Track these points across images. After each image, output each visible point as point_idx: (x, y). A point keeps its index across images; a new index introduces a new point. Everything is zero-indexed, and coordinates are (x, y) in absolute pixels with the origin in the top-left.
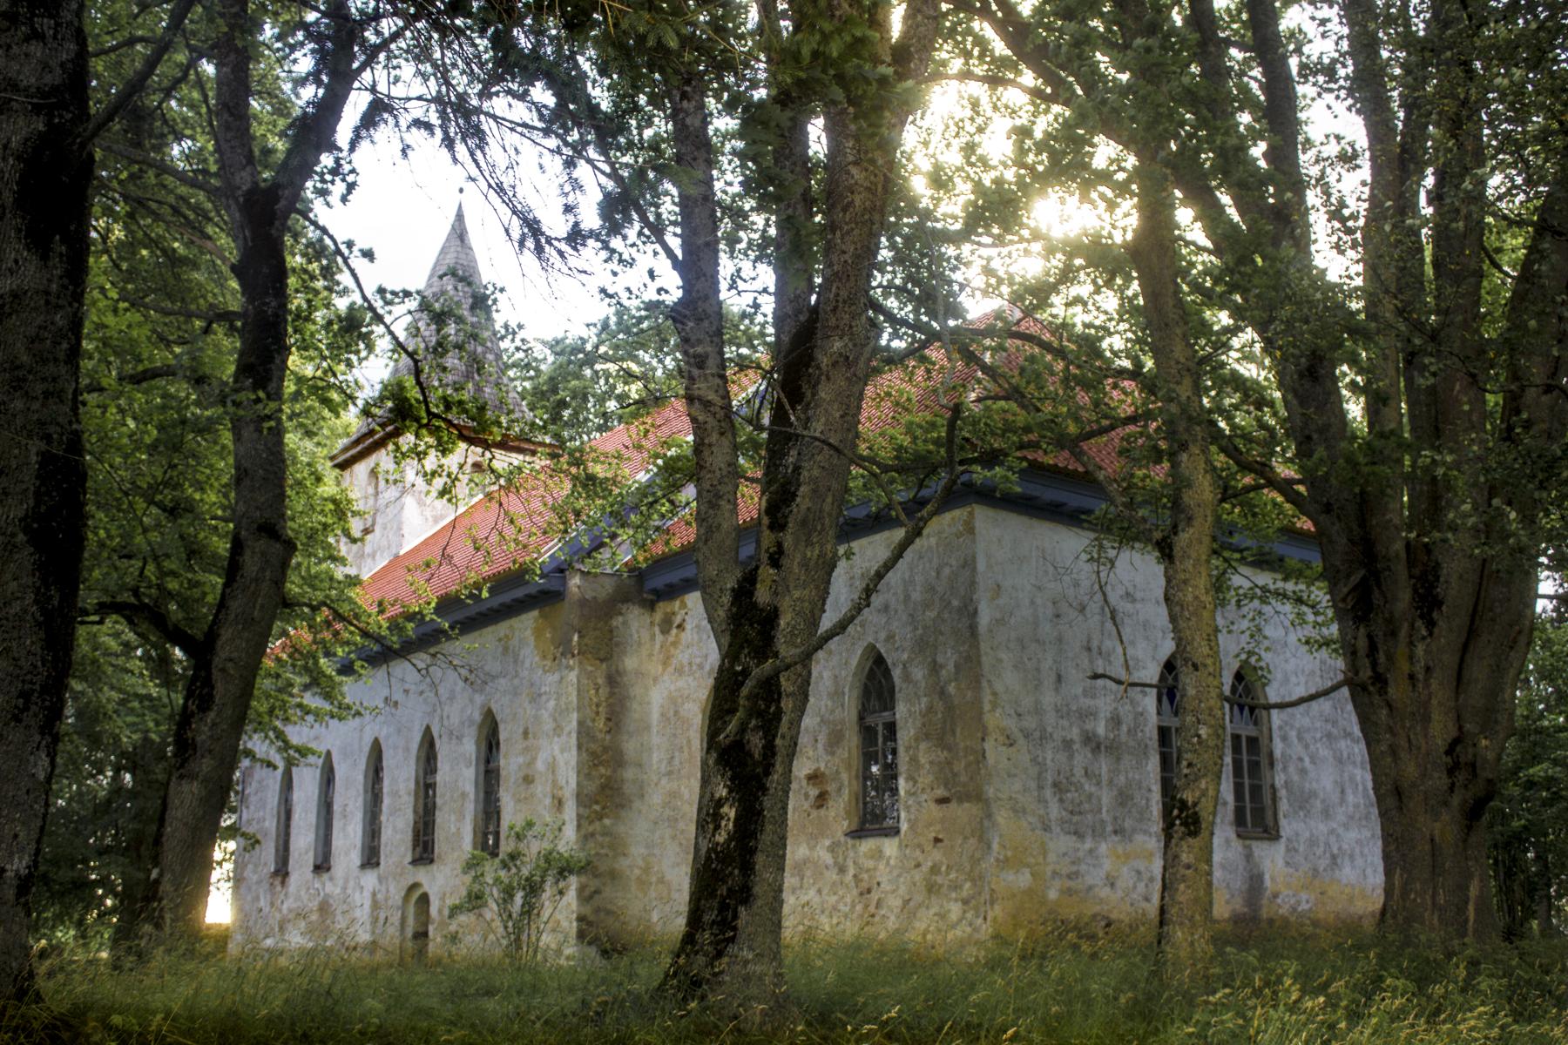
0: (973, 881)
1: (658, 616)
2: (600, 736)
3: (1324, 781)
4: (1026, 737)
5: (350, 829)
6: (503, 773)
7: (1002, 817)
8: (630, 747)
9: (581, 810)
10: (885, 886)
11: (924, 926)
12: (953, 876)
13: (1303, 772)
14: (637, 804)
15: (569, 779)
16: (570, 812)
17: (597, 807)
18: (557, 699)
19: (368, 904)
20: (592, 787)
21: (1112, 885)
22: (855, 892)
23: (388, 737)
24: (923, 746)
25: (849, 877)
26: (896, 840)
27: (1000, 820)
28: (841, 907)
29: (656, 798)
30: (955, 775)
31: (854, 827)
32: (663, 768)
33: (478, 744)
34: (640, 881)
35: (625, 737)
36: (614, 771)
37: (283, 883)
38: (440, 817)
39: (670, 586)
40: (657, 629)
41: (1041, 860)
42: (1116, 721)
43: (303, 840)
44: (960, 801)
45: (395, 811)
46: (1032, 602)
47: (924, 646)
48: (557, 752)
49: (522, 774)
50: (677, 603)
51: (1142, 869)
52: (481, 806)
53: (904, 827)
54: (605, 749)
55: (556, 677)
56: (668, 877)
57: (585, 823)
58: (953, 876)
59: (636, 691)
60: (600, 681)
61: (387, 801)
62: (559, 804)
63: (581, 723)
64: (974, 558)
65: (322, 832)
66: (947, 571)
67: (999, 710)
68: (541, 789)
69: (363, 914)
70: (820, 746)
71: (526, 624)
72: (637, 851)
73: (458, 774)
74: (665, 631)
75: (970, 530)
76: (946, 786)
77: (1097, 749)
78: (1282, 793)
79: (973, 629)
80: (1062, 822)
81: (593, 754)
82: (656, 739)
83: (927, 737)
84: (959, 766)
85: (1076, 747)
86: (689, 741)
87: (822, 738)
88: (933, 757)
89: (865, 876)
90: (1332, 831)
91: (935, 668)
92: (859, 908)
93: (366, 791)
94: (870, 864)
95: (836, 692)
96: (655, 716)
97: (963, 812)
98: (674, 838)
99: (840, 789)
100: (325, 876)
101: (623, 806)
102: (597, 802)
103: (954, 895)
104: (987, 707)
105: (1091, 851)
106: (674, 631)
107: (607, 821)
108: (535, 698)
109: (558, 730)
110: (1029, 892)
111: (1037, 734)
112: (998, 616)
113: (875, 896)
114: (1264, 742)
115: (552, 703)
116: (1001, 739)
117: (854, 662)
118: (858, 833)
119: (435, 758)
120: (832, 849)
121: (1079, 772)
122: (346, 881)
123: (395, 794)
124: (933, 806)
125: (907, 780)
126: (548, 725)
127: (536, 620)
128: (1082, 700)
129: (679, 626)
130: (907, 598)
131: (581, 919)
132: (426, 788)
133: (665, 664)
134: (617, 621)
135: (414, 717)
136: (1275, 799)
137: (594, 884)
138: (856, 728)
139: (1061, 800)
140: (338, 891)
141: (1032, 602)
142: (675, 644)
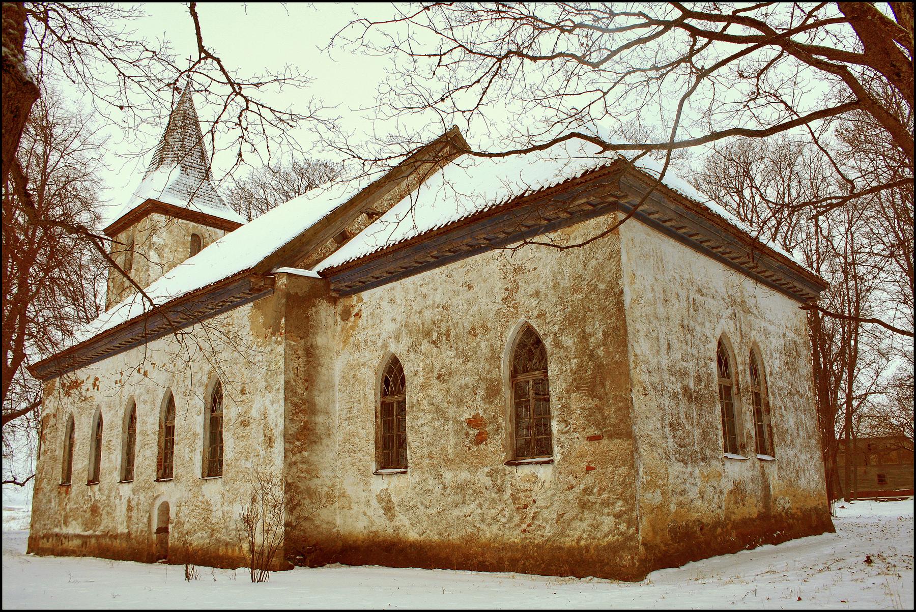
0: (626, 501)
1: (339, 308)
2: (300, 391)
3: (790, 421)
4: (654, 389)
5: (113, 457)
7: (644, 448)
8: (320, 400)
11: (578, 533)
12: (605, 495)
13: (782, 416)
14: (325, 441)
16: (279, 446)
17: (298, 443)
19: (124, 507)
20: (294, 428)
21: (702, 497)
22: (513, 507)
23: (139, 396)
24: (574, 396)
25: (507, 496)
26: (550, 468)
27: (642, 451)
29: (339, 437)
30: (605, 418)
32: (344, 414)
34: (328, 496)
36: (310, 417)
37: (67, 492)
41: (665, 482)
42: (698, 378)
43: (81, 464)
44: (611, 437)
45: (145, 445)
46: (653, 289)
48: (268, 404)
51: (716, 485)
52: (207, 443)
57: (290, 454)
58: (605, 495)
59: (325, 360)
60: (299, 352)
61: (138, 438)
62: (270, 442)
63: (286, 382)
64: (619, 251)
65: (93, 459)
66: (593, 263)
67: (638, 368)
69: (121, 510)
70: (478, 397)
72: (325, 473)
76: (597, 426)
77: (690, 399)
78: (775, 430)
79: (620, 306)
81: (295, 405)
82: (338, 395)
83: (578, 388)
84: (610, 411)
86: (365, 397)
87: (480, 394)
89: (522, 495)
90: (795, 455)
91: (584, 337)
92: (516, 519)
93: (124, 432)
95: (493, 357)
96: (337, 379)
98: (353, 465)
99: (497, 429)
100: (96, 488)
101: (315, 442)
102: (298, 440)
103: (606, 511)
104: (632, 365)
105: (691, 474)
106: (352, 319)
107: (305, 453)
109: (269, 388)
110: (660, 507)
111: (659, 387)
112: (635, 297)
113: (531, 511)
114: (763, 396)
116: (641, 389)
119: (174, 410)
120: (490, 475)
121: (682, 416)
122: (110, 491)
125: (559, 422)
127: (251, 311)
128: (682, 362)
129: (356, 315)
130: (556, 285)
132: (168, 432)
133: (345, 342)
136: (771, 435)
138: (509, 384)
139: (674, 436)
140: (105, 498)
141: (653, 289)
142: (353, 328)
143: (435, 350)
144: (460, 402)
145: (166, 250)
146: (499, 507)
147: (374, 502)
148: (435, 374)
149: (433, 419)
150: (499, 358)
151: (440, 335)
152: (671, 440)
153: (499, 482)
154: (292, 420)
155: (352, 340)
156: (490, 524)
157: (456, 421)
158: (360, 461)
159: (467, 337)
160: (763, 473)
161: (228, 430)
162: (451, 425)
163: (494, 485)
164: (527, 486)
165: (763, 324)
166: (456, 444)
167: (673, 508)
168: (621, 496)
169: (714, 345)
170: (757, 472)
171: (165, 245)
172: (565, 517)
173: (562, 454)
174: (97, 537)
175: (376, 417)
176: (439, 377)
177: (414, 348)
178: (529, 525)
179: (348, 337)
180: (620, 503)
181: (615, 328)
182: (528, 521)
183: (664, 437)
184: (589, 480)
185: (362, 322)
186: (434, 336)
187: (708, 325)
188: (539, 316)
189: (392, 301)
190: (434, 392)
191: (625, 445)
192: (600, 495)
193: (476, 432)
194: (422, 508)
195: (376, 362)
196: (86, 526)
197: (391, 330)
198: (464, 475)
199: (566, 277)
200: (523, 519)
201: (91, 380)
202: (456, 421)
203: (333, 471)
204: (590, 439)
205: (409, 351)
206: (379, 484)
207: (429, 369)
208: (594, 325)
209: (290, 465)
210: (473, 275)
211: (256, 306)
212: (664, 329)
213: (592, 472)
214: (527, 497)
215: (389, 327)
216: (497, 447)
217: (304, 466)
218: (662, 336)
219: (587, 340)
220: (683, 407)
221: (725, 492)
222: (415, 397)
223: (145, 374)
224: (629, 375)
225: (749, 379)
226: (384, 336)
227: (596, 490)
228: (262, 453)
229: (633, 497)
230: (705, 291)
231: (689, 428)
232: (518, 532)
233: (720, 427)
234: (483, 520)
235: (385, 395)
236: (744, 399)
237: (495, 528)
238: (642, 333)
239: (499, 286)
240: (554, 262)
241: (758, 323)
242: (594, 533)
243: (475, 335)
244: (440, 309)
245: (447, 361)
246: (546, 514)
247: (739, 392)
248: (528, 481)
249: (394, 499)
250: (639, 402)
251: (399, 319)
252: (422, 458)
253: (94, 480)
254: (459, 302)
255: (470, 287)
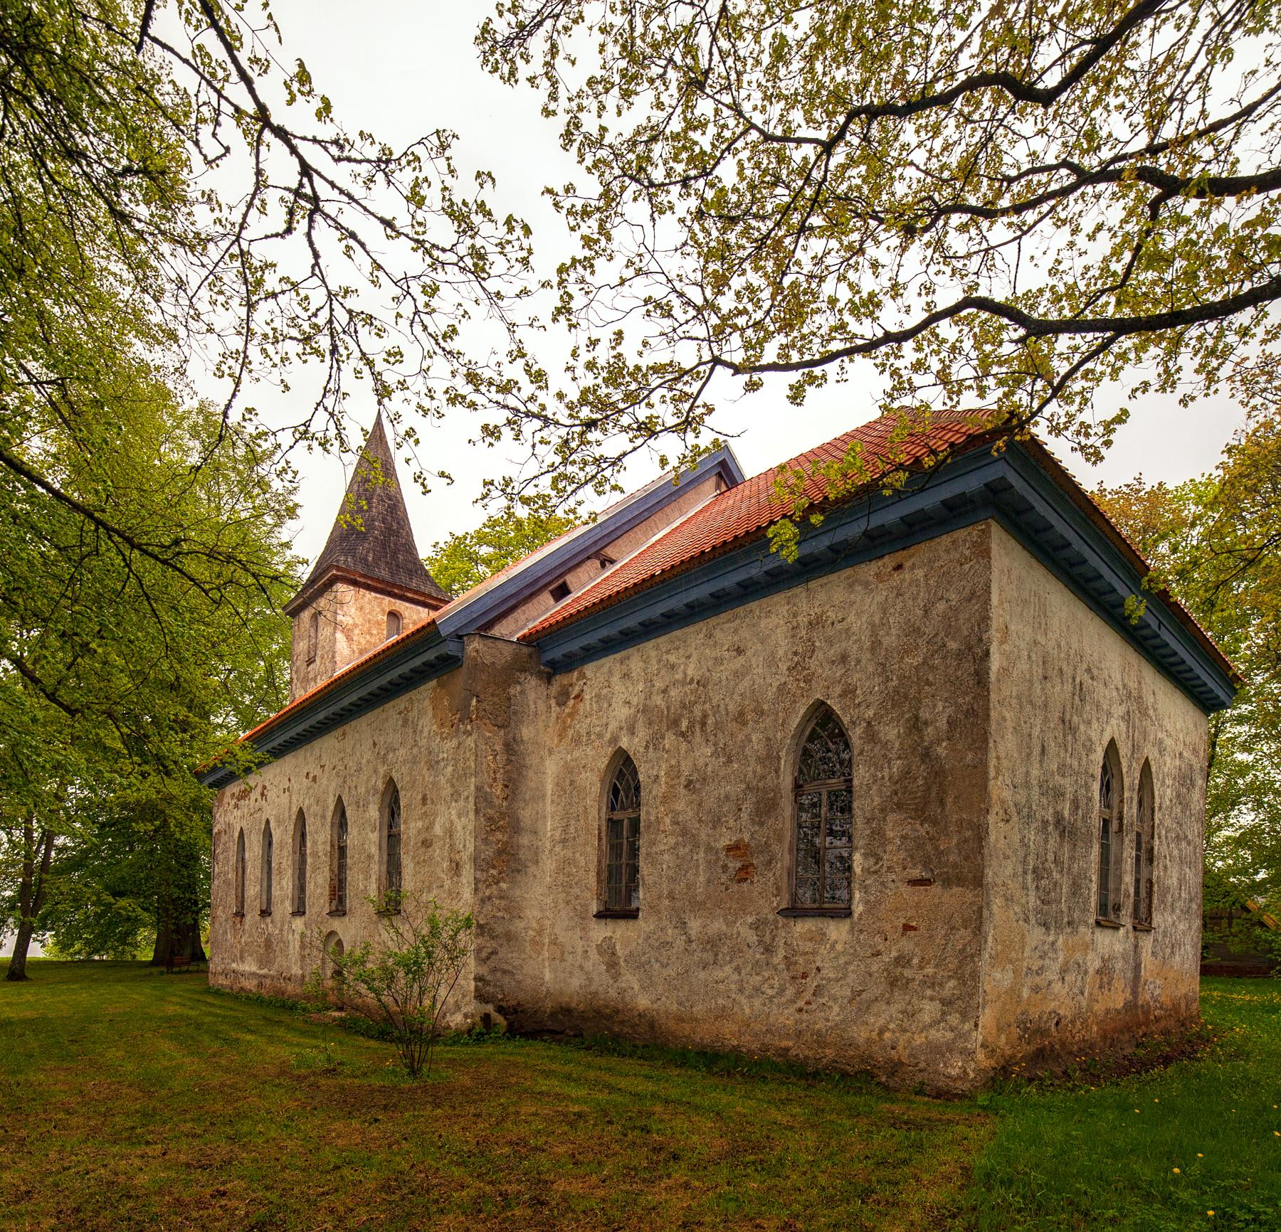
1: (555, 689)
2: (497, 802)
6: (404, 837)
7: (997, 903)
8: (526, 814)
9: (479, 874)
10: (828, 973)
11: (881, 1022)
12: (929, 970)
14: (532, 869)
15: (467, 845)
18: (455, 765)
20: (489, 852)
22: (786, 975)
24: (892, 817)
25: (778, 959)
28: (765, 987)
31: (784, 906)
33: (380, 810)
35: (522, 804)
38: (350, 876)
39: (568, 656)
40: (553, 702)
42: (1075, 805)
44: (947, 883)
47: (903, 699)
48: (454, 817)
49: (421, 838)
50: (576, 674)
53: (858, 908)
54: (503, 815)
55: (454, 742)
56: (561, 939)
58: (929, 970)
59: (532, 760)
60: (497, 748)
62: (456, 868)
63: (478, 789)
66: (941, 606)
68: (437, 852)
70: (744, 816)
71: (423, 698)
73: (365, 837)
74: (561, 704)
75: (985, 553)
76: (926, 865)
77: (1062, 835)
78: (1155, 888)
79: (981, 678)
80: (1038, 911)
82: (549, 808)
83: (899, 806)
85: (1050, 828)
87: (748, 806)
88: (907, 830)
91: (916, 725)
92: (790, 992)
94: (809, 946)
95: (768, 756)
97: (952, 898)
98: (568, 903)
99: (770, 862)
100: (268, 920)
102: (494, 867)
103: (929, 992)
104: (992, 773)
105: (1053, 944)
107: (504, 885)
108: (432, 765)
109: (456, 795)
113: (812, 983)
115: (450, 769)
117: (795, 722)
118: (794, 912)
120: (756, 926)
121: (1050, 857)
123: (315, 854)
124: (906, 890)
125: (865, 856)
126: (447, 791)
127: (434, 689)
129: (577, 697)
130: (876, 644)
131: (478, 979)
134: (515, 690)
135: (329, 788)
137: (491, 945)
142: (571, 715)
143: (684, 746)
144: (717, 822)
145: (357, 631)
146: (766, 974)
147: (593, 954)
148: (683, 781)
149: (677, 843)
150: (779, 758)
151: (691, 727)
152: (1032, 893)
153: (767, 938)
154: (485, 841)
155: (570, 732)
156: (750, 997)
157: (709, 849)
158: (577, 897)
159: (732, 726)
160: (1136, 946)
161: (407, 853)
162: (702, 855)
163: (760, 942)
164: (809, 946)
165: (1160, 735)
166: (709, 881)
167: (1025, 993)
168: (957, 974)
169: (1098, 756)
170: (1129, 945)
171: (355, 625)
172: (864, 996)
173: (867, 902)
174: (273, 978)
175: (600, 839)
176: (688, 785)
177: (654, 742)
178: (808, 1003)
179: (565, 729)
180: (952, 983)
181: (970, 713)
182: (807, 996)
183: (1025, 887)
184: (907, 945)
185: (585, 706)
186: (684, 724)
187: (1095, 725)
188: (844, 694)
189: (626, 676)
190: (680, 806)
191: (969, 896)
192: (921, 968)
193: (739, 865)
194: (657, 966)
195: (603, 763)
196: (262, 963)
197: (623, 717)
198: (718, 926)
199: (894, 631)
200: (799, 993)
201: (259, 789)
202: (709, 849)
203: (542, 910)
204: (914, 882)
205: (647, 747)
206: (601, 931)
207: (674, 772)
208: (935, 706)
209: (483, 901)
210: (745, 633)
211: (440, 685)
212: (1038, 721)
213: (912, 933)
214: (807, 962)
215: (621, 713)
216: (767, 891)
217: (503, 902)
218: (1036, 732)
219: (920, 731)
220: (1052, 844)
221: (1091, 971)
222: (653, 812)
223: (314, 779)
224: (986, 787)
225: (1135, 811)
226: (613, 726)
227: (915, 961)
228: (447, 883)
229: (975, 976)
230: (1095, 672)
231: (1056, 875)
232: (792, 1010)
233: (1094, 878)
234: (741, 991)
235: (613, 809)
236: (1127, 840)
237: (757, 1003)
238: (1009, 724)
239: (783, 644)
240: (874, 607)
241: (1155, 733)
242: (906, 1024)
243: (744, 723)
244: (694, 685)
245: (701, 762)
246: (835, 990)
247: (1120, 830)
248: (811, 940)
249: (620, 953)
250: (999, 834)
251: (635, 701)
252: (659, 897)
253: (265, 913)
254: (722, 673)
255: (740, 651)
